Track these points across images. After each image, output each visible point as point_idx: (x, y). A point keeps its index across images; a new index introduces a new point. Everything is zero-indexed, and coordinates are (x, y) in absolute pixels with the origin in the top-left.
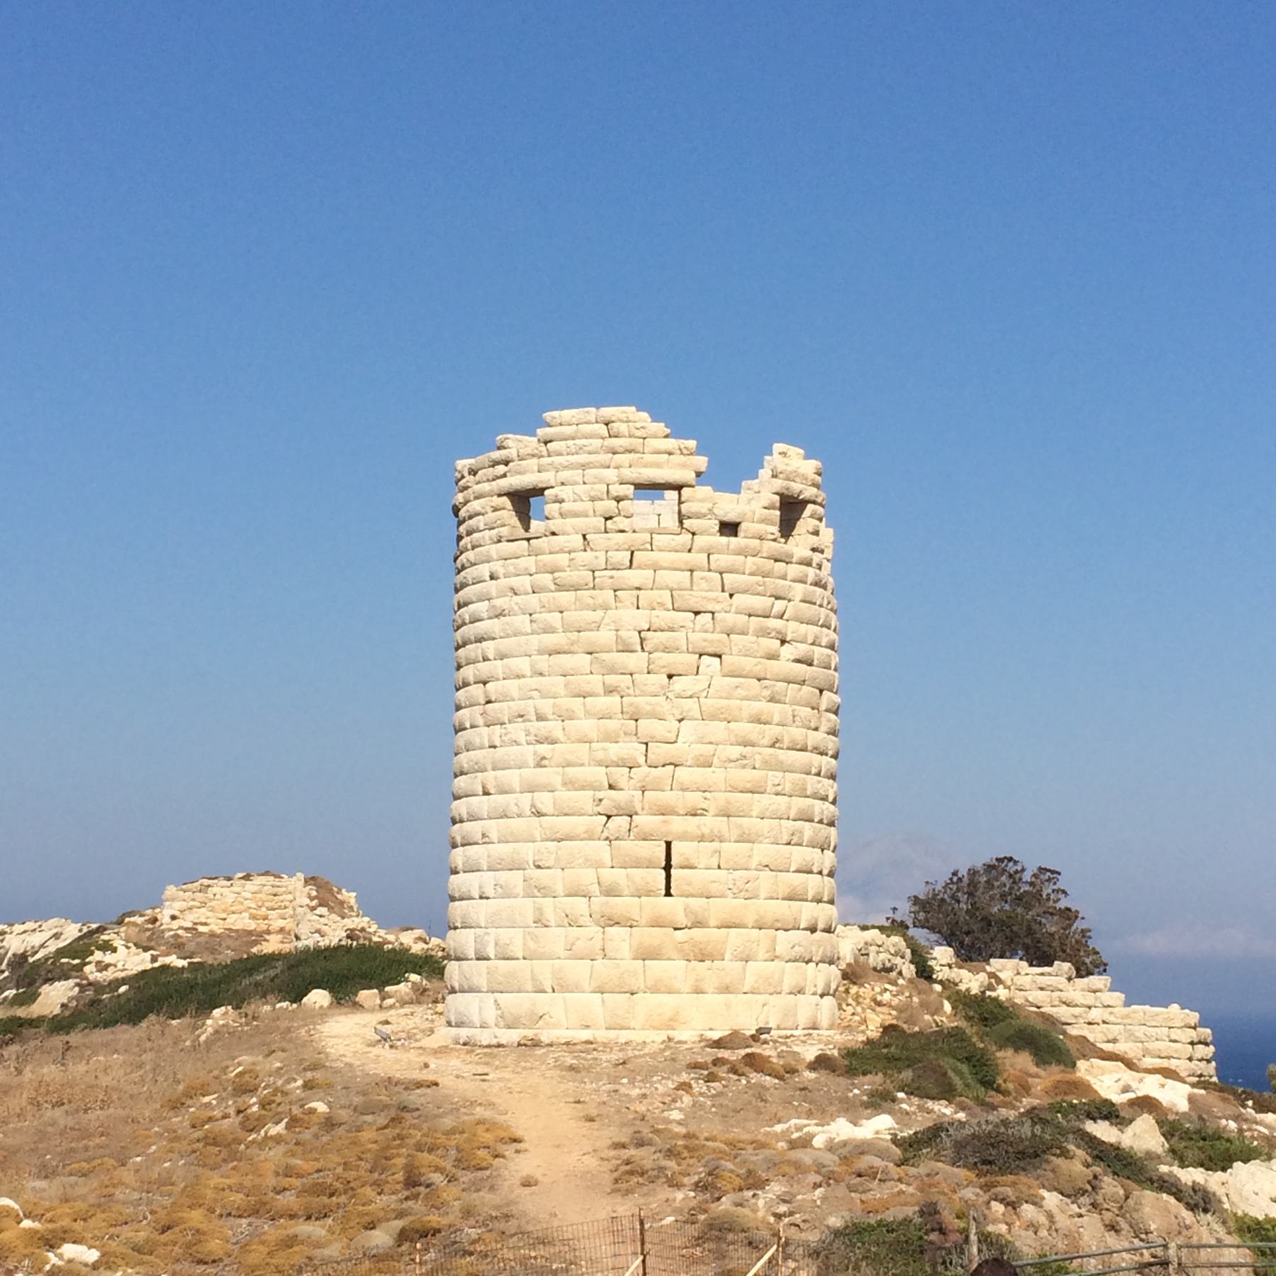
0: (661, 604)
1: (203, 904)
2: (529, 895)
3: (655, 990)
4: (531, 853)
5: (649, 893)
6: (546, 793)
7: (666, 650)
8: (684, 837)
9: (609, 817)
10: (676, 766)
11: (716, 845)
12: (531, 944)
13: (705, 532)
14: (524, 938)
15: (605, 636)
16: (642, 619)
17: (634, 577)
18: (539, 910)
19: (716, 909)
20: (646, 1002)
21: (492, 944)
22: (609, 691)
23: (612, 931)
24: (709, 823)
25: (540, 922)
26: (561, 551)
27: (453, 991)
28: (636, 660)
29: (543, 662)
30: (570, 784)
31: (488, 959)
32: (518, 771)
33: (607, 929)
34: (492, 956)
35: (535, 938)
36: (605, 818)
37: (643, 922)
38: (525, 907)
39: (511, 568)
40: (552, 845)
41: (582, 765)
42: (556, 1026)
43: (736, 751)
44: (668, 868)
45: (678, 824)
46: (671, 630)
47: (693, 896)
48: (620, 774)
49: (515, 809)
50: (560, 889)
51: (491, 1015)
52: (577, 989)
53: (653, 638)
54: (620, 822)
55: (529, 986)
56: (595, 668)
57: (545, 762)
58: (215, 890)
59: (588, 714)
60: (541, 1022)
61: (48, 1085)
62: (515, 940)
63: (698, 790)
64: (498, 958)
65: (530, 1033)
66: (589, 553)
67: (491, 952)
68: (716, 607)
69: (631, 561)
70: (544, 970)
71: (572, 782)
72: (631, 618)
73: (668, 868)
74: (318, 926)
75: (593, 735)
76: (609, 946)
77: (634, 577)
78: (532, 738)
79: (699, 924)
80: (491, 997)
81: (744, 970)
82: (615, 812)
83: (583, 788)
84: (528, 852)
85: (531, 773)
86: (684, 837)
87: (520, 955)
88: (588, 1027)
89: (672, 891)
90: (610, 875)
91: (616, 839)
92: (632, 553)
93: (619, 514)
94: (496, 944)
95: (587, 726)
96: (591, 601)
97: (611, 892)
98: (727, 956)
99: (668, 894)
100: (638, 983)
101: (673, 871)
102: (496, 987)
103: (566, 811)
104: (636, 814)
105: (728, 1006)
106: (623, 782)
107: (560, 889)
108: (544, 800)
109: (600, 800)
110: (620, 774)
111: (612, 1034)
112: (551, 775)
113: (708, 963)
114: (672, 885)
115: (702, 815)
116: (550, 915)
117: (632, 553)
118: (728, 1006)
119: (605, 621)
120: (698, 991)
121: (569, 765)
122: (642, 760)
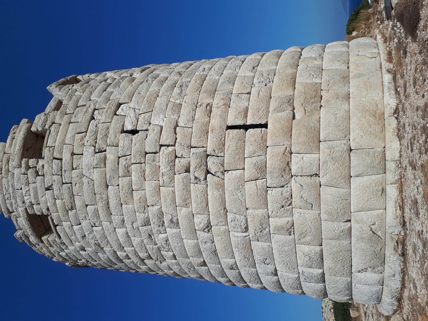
0: (82, 139)
3: (347, 135)
4: (236, 234)
7: (106, 136)
9: (208, 172)
10: (177, 126)
12: (308, 238)
14: (304, 244)
15: (96, 175)
16: (88, 151)
17: (66, 156)
18: (279, 229)
20: (356, 138)
21: (311, 270)
22: (128, 174)
24: (217, 101)
25: (290, 230)
26: (55, 204)
28: (111, 156)
29: (116, 219)
30: (186, 203)
31: (323, 274)
32: (185, 241)
33: (293, 172)
34: (321, 271)
35: (303, 235)
36: (209, 175)
37: (287, 143)
38: (278, 240)
39: (73, 237)
40: (230, 216)
41: (174, 192)
43: (176, 90)
44: (246, 127)
45: (215, 121)
46: (96, 132)
47: (268, 108)
48: (179, 164)
49: (209, 244)
50: (261, 212)
51: (372, 276)
52: (346, 199)
53: (100, 144)
55: (345, 242)
57: (174, 220)
58: (325, 316)
60: (379, 233)
61: (364, 305)
62: (305, 250)
63: (195, 110)
64: (321, 266)
65: (390, 246)
66: (54, 187)
67: (317, 271)
68: (92, 107)
69: (57, 159)
70: (329, 228)
71: (185, 200)
72: (88, 158)
73: (246, 127)
75: (154, 183)
76: (307, 171)
77: (66, 156)
78: (161, 229)
79: (290, 101)
80: (357, 276)
81: (326, 70)
83: (189, 191)
84: (236, 236)
85: (183, 230)
87: (318, 248)
88: (383, 191)
89: (263, 122)
90: (249, 171)
91: (223, 165)
93: (36, 167)
94: (310, 267)
95: (149, 186)
96: (78, 185)
97: (262, 169)
98: (318, 81)
99: (265, 126)
100: (341, 145)
102: (347, 270)
103: (204, 204)
104: (206, 151)
105: (359, 76)
106: (184, 161)
107: (261, 212)
108: (199, 221)
110: (179, 164)
112: (183, 212)
113: (323, 93)
115: (211, 107)
116: (283, 221)
118: (359, 76)
122: (171, 149)
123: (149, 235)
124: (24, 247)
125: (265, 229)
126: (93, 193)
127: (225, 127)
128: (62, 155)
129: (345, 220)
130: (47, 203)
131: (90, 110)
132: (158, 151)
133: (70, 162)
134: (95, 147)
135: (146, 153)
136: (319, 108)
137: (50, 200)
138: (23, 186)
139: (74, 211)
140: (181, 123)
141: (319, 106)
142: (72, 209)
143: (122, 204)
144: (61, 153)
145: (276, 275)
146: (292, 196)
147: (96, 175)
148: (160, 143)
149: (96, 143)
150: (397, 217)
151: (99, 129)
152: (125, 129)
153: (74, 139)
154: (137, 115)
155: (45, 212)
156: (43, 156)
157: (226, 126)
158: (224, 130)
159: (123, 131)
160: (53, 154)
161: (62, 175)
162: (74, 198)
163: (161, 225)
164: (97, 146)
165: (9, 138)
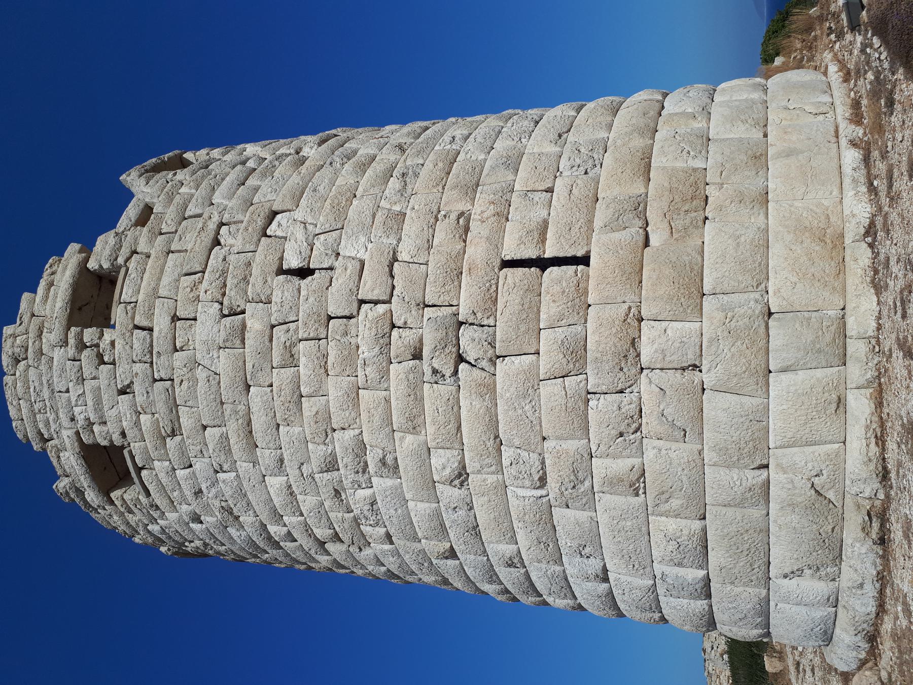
0: (195, 286)
1: (718, 677)
2: (590, 503)
4: (521, 492)
5: (581, 290)
6: (433, 461)
8: (496, 240)
9: (461, 359)
10: (395, 259)
11: (515, 198)
12: (675, 503)
13: (136, 240)
14: (666, 514)
15: (224, 363)
16: (208, 312)
17: (161, 323)
18: (613, 484)
19: (615, 185)
20: (781, 288)
21: (681, 571)
22: (291, 360)
23: (647, 353)
25: (636, 484)
26: (137, 423)
27: (768, 634)
28: (255, 323)
29: (266, 456)
30: (414, 425)
31: (707, 581)
33: (645, 360)
34: (702, 573)
35: (664, 495)
36: (463, 366)
37: (631, 298)
38: (610, 505)
39: (175, 494)
40: (507, 454)
41: (388, 401)
42: (838, 462)
43: (394, 184)
44: (542, 264)
48: (400, 340)
49: (462, 513)
50: (573, 445)
51: (814, 587)
53: (233, 297)
54: (470, 342)
55: (756, 513)
56: (263, 379)
57: (389, 460)
58: (710, 669)
59: (319, 392)
60: (831, 495)
62: (668, 528)
63: (433, 227)
64: (704, 561)
66: (136, 387)
67: (695, 574)
68: (216, 218)
70: (721, 481)
71: (411, 419)
72: (207, 327)
73: (542, 264)
74: (718, 655)
75: (346, 381)
76: (675, 359)
77: (161, 323)
78: (361, 478)
79: (639, 207)
80: (780, 585)
81: (716, 140)
82: (451, 348)
84: (521, 496)
86: (496, 240)
87: (697, 525)
88: (841, 402)
89: (580, 254)
92: (137, 327)
93: (97, 346)
94: (680, 565)
95: (336, 387)
96: (185, 384)
98: (699, 164)
99: (584, 260)
100: (747, 304)
101: (547, 255)
103: (452, 427)
104: (456, 315)
105: (789, 153)
106: (409, 336)
107: (573, 445)
108: (442, 462)
109: (435, 372)
110: (400, 340)
111: (857, 348)
112: (406, 444)
114: (569, 254)
115: (468, 221)
116: (622, 465)
117: (137, 327)
118: (789, 153)
119: (208, 365)
120: (764, 198)
121: (388, 420)
122: (381, 308)
123: (336, 490)
124: (74, 513)
125: (582, 482)
126: (218, 400)
127: (497, 263)
128: (152, 321)
129: (756, 464)
130: (121, 421)
131: (212, 226)
132: (355, 313)
133: (170, 336)
134: (222, 304)
135: (330, 318)
136: (700, 223)
137: (128, 416)
138: (71, 385)
139: (178, 438)
140: (403, 254)
141: (702, 217)
142: (173, 434)
143: (278, 425)
144: (150, 316)
145: (606, 579)
146: (641, 411)
147: (224, 363)
148: (360, 297)
149: (224, 294)
150: (870, 460)
151: (231, 267)
152: (285, 267)
153: (178, 288)
154: (311, 238)
155: (117, 440)
156: (112, 322)
157: (499, 261)
158: (496, 270)
159: (281, 271)
160: (133, 318)
161: (152, 363)
162: (177, 412)
163: (361, 470)
164: (226, 302)
165: (43, 283)
